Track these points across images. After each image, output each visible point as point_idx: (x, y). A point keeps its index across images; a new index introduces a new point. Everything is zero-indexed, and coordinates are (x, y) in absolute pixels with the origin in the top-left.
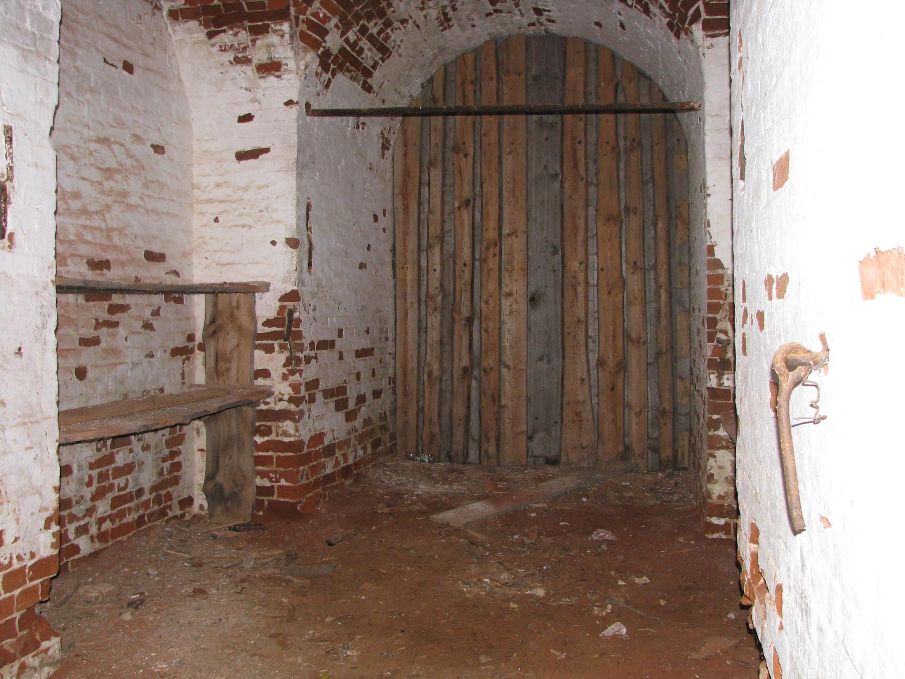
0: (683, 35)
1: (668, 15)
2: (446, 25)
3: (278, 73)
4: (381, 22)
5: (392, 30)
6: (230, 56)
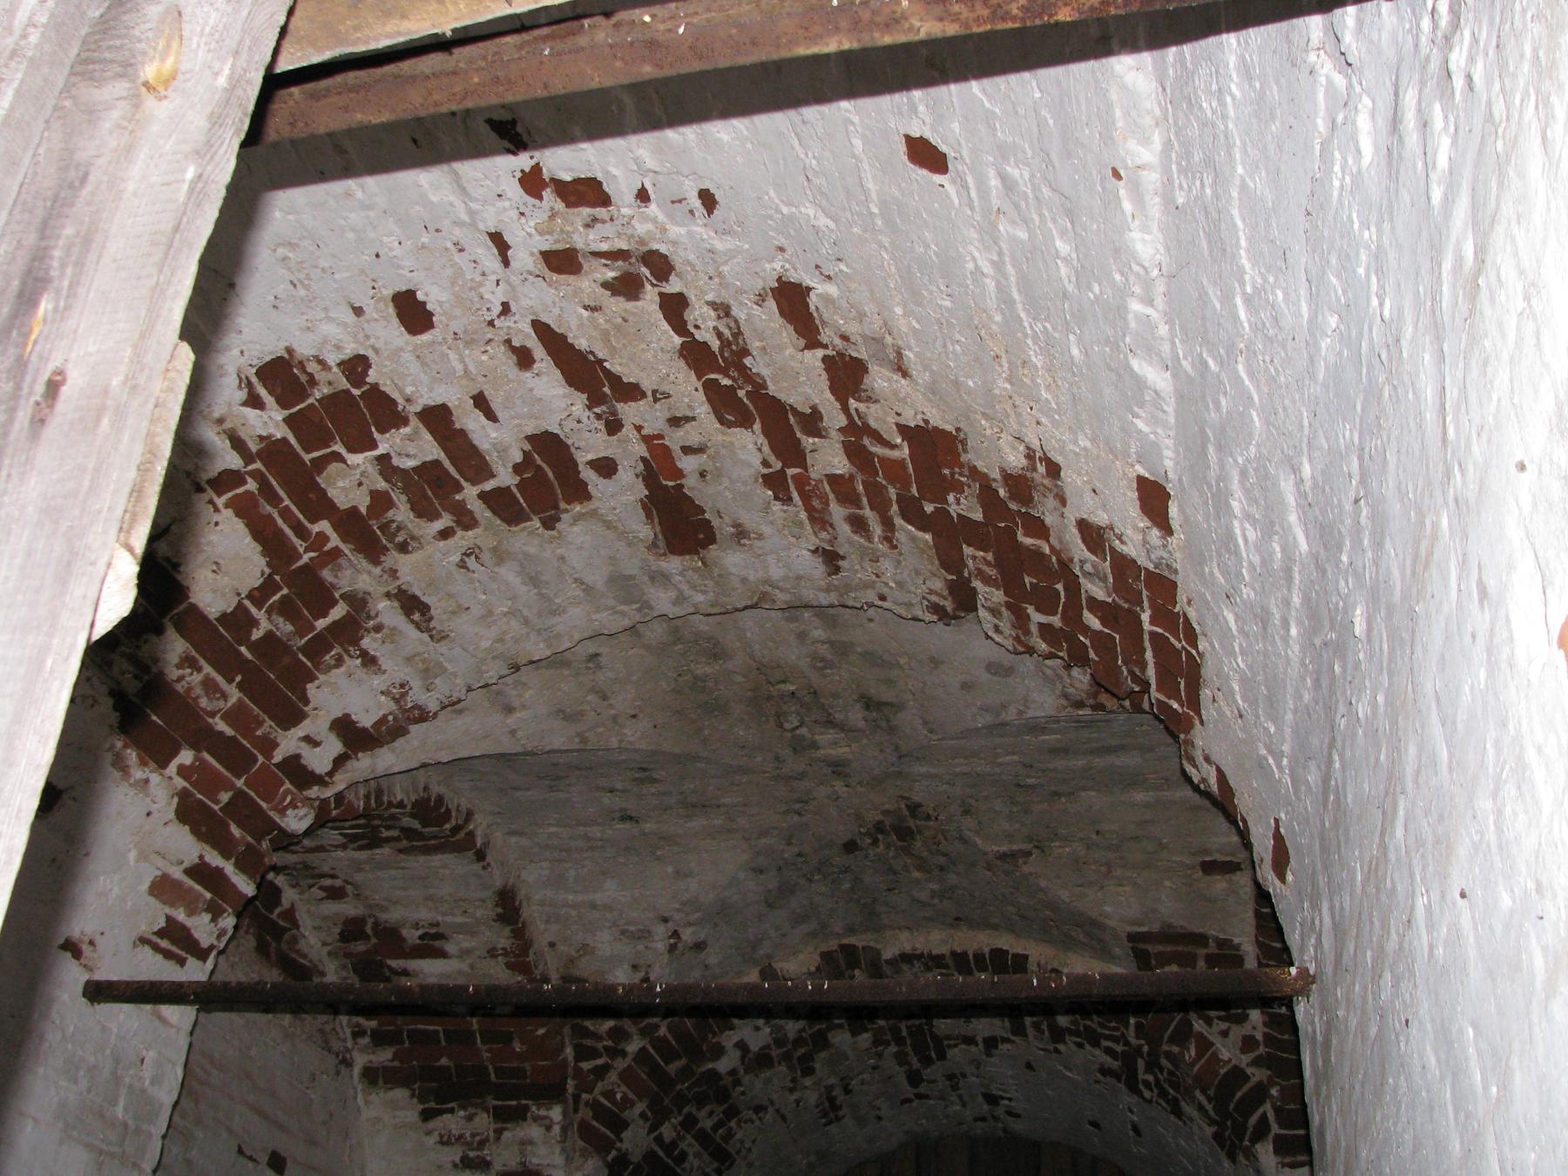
0: (1241, 1158)
1: (1212, 1122)
2: (832, 1115)
3: (662, 543)
4: (720, 1110)
5: (738, 1125)
6: (455, 1154)
